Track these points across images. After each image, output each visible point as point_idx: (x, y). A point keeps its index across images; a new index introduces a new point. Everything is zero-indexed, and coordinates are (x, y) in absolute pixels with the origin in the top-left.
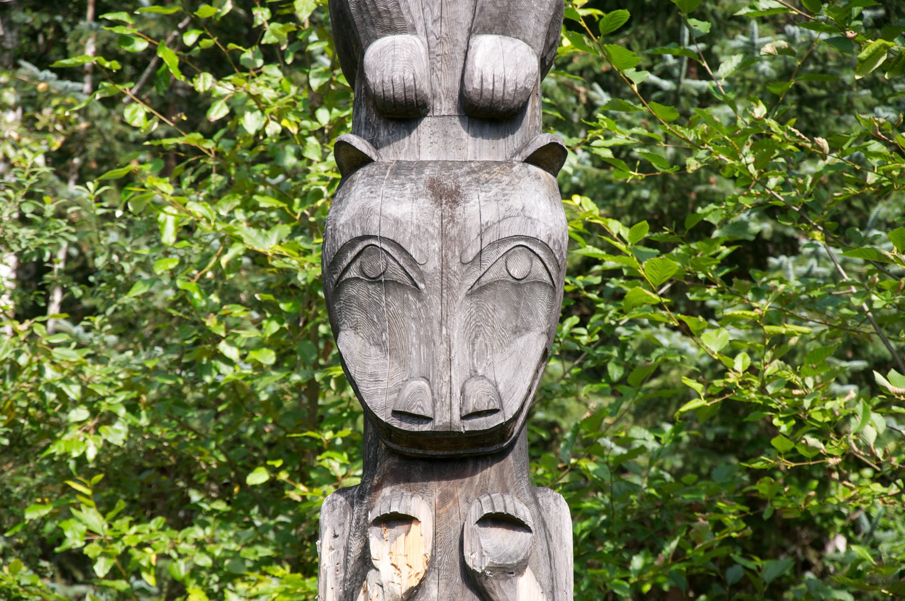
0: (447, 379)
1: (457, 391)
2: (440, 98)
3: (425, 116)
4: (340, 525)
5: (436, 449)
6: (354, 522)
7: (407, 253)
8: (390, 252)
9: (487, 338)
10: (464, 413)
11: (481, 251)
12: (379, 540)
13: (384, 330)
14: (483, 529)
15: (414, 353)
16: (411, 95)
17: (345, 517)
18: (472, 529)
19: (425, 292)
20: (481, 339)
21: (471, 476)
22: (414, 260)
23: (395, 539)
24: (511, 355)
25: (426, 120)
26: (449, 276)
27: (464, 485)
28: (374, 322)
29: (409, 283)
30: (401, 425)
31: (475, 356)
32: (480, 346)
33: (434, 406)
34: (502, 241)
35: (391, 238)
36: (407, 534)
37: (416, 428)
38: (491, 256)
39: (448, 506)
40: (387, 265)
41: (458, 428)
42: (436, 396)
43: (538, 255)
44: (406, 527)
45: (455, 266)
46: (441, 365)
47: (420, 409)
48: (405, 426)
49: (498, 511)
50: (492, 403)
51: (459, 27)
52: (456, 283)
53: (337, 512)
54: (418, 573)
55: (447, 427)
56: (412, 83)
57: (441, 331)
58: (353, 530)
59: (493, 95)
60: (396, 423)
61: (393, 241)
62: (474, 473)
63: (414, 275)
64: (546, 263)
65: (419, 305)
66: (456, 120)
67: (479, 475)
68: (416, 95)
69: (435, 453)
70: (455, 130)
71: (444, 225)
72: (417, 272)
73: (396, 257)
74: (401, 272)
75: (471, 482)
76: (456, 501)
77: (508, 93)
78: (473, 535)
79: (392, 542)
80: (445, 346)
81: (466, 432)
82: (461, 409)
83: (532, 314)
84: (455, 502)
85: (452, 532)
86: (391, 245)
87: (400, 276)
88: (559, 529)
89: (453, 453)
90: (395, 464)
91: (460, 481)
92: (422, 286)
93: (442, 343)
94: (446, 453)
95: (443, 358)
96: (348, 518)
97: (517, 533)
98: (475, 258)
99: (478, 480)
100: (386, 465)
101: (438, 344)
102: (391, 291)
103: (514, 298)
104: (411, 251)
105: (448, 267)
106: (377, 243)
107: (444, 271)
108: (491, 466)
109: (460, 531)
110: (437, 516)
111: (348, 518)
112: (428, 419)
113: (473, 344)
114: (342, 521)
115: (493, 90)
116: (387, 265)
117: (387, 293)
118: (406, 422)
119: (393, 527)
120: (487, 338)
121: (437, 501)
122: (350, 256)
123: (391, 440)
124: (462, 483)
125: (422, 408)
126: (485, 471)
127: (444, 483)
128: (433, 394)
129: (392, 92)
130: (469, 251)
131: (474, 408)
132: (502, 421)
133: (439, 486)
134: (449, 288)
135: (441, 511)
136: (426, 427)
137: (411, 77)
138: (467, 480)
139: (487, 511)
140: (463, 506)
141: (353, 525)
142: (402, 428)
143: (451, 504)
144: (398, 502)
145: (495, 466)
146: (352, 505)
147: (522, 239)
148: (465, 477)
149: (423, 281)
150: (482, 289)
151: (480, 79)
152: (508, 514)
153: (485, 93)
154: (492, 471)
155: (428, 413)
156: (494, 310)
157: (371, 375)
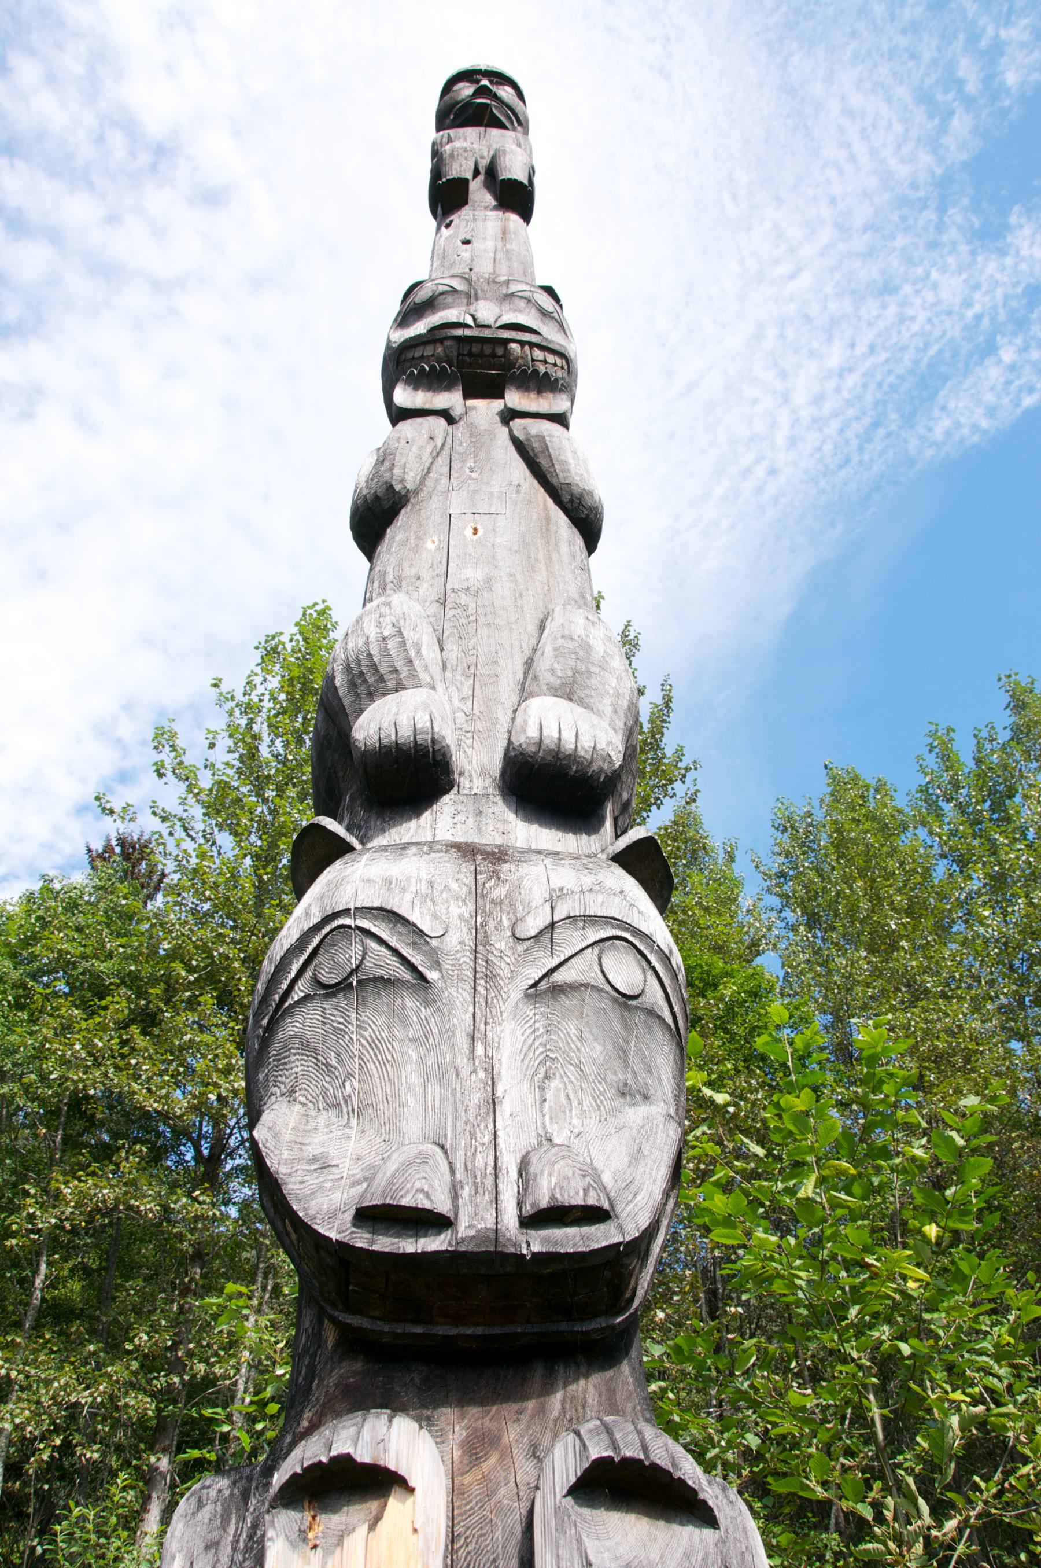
0: (487, 1138)
1: (510, 1164)
2: (470, 776)
3: (446, 792)
4: (207, 1548)
5: (457, 1320)
6: (244, 1535)
7: (405, 921)
8: (374, 930)
9: (569, 1087)
10: (528, 1210)
11: (552, 925)
12: (293, 1545)
13: (350, 1075)
14: (586, 1511)
15: (411, 1102)
16: (424, 739)
17: (224, 1527)
18: (557, 1509)
19: (440, 984)
20: (555, 1084)
21: (540, 1396)
22: (421, 933)
23: (340, 1542)
24: (618, 1130)
25: (446, 799)
26: (491, 957)
27: (525, 1417)
28: (327, 1065)
29: (407, 976)
30: (372, 1242)
31: (546, 1110)
32: (557, 1096)
33: (455, 1195)
34: (591, 920)
35: (376, 905)
36: (372, 1527)
37: (410, 1246)
38: (571, 940)
39: (486, 1466)
40: (365, 954)
41: (515, 1245)
42: (460, 1175)
43: (654, 969)
44: (373, 1505)
45: (501, 942)
46: (472, 1111)
47: (421, 1196)
48: (384, 1243)
49: (628, 1453)
50: (592, 1193)
51: (500, 707)
52: (503, 970)
53: (207, 1511)
54: (427, 1195)
55: (486, 1239)
56: (428, 724)
57: (473, 1050)
58: (240, 1557)
59: (559, 746)
60: (361, 1239)
61: (380, 909)
62: (547, 1390)
63: (416, 959)
64: (669, 990)
65: (425, 1013)
66: (498, 799)
67: (559, 1396)
68: (433, 741)
69: (453, 1331)
70: (495, 809)
71: (480, 882)
72: (425, 954)
73: (384, 936)
74: (393, 961)
75: (542, 1410)
76: (506, 1453)
77: (583, 748)
78: (561, 1528)
79: (328, 1553)
80: (482, 1075)
81: (535, 1255)
82: (520, 1204)
83: (650, 1072)
84: (502, 1457)
85: (498, 1534)
86: (376, 918)
87: (394, 969)
88: (748, 1557)
89: (496, 1331)
90: (355, 1373)
91: (515, 1407)
92: (432, 975)
93: (474, 1071)
94: (480, 1331)
95: (476, 1098)
96: (232, 1529)
97: (676, 1528)
98: (541, 933)
99: (558, 1406)
100: (332, 1380)
101: (465, 1072)
102: (370, 998)
103: (618, 1026)
104: (415, 917)
105: (487, 942)
106: (347, 921)
107: (480, 948)
108: (587, 1376)
109: (518, 1530)
110: (456, 1492)
111: (232, 1529)
112: (439, 1222)
113: (542, 1089)
114: (215, 1536)
115: (560, 739)
116: (365, 954)
117: (361, 1004)
118: (385, 1235)
119: (335, 1510)
120: (569, 1087)
121: (457, 1453)
122: (295, 968)
123: (348, 1309)
124: (520, 1412)
125: (427, 1195)
126: (573, 1387)
127: (474, 1411)
128: (453, 1171)
129: (393, 738)
130: (529, 919)
131: (553, 1197)
132: (617, 1239)
133: (462, 1417)
134: (491, 977)
135: (468, 1479)
136: (435, 1243)
137: (427, 718)
138: (531, 1405)
139: (598, 1451)
140: (525, 1470)
141: (241, 1545)
142: (376, 1247)
143: (493, 1460)
144: (353, 1430)
145: (596, 1379)
146: (245, 1496)
147: (626, 930)
148: (525, 1397)
149: (437, 965)
150: (559, 990)
151: (537, 726)
152: (654, 1466)
153: (546, 742)
154: (591, 1389)
155: (442, 1205)
156: (581, 1038)
157: (315, 1159)
